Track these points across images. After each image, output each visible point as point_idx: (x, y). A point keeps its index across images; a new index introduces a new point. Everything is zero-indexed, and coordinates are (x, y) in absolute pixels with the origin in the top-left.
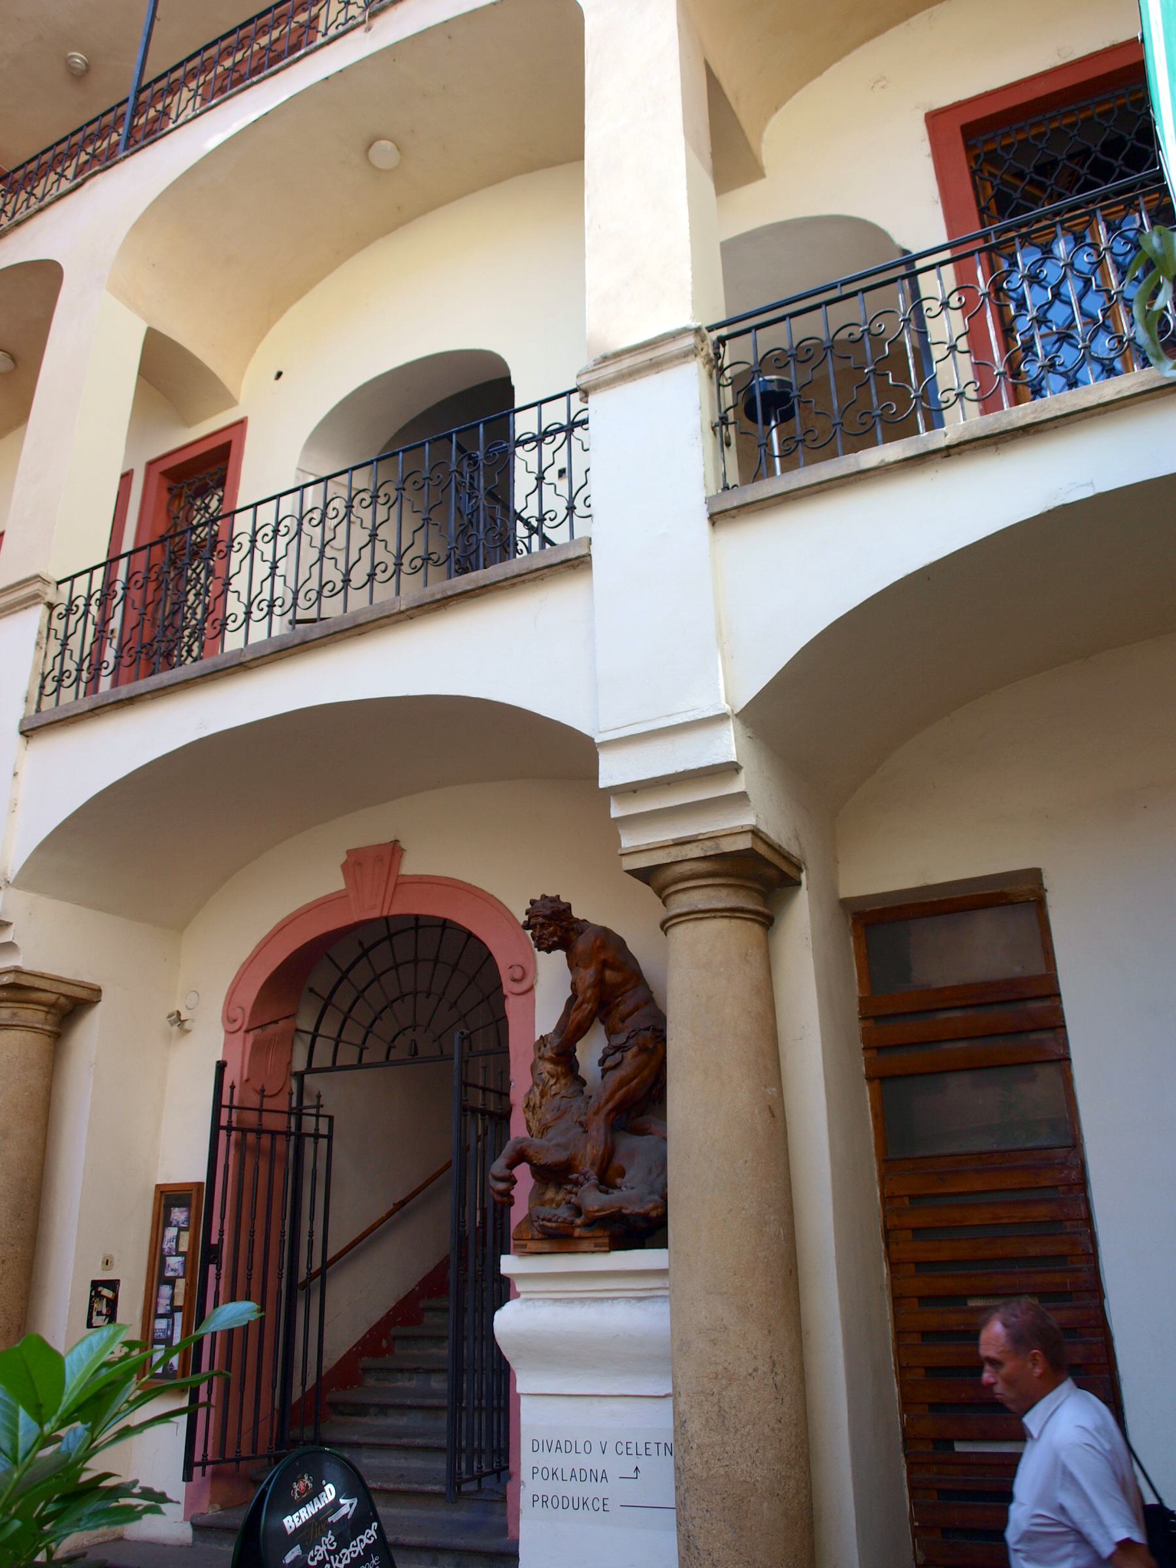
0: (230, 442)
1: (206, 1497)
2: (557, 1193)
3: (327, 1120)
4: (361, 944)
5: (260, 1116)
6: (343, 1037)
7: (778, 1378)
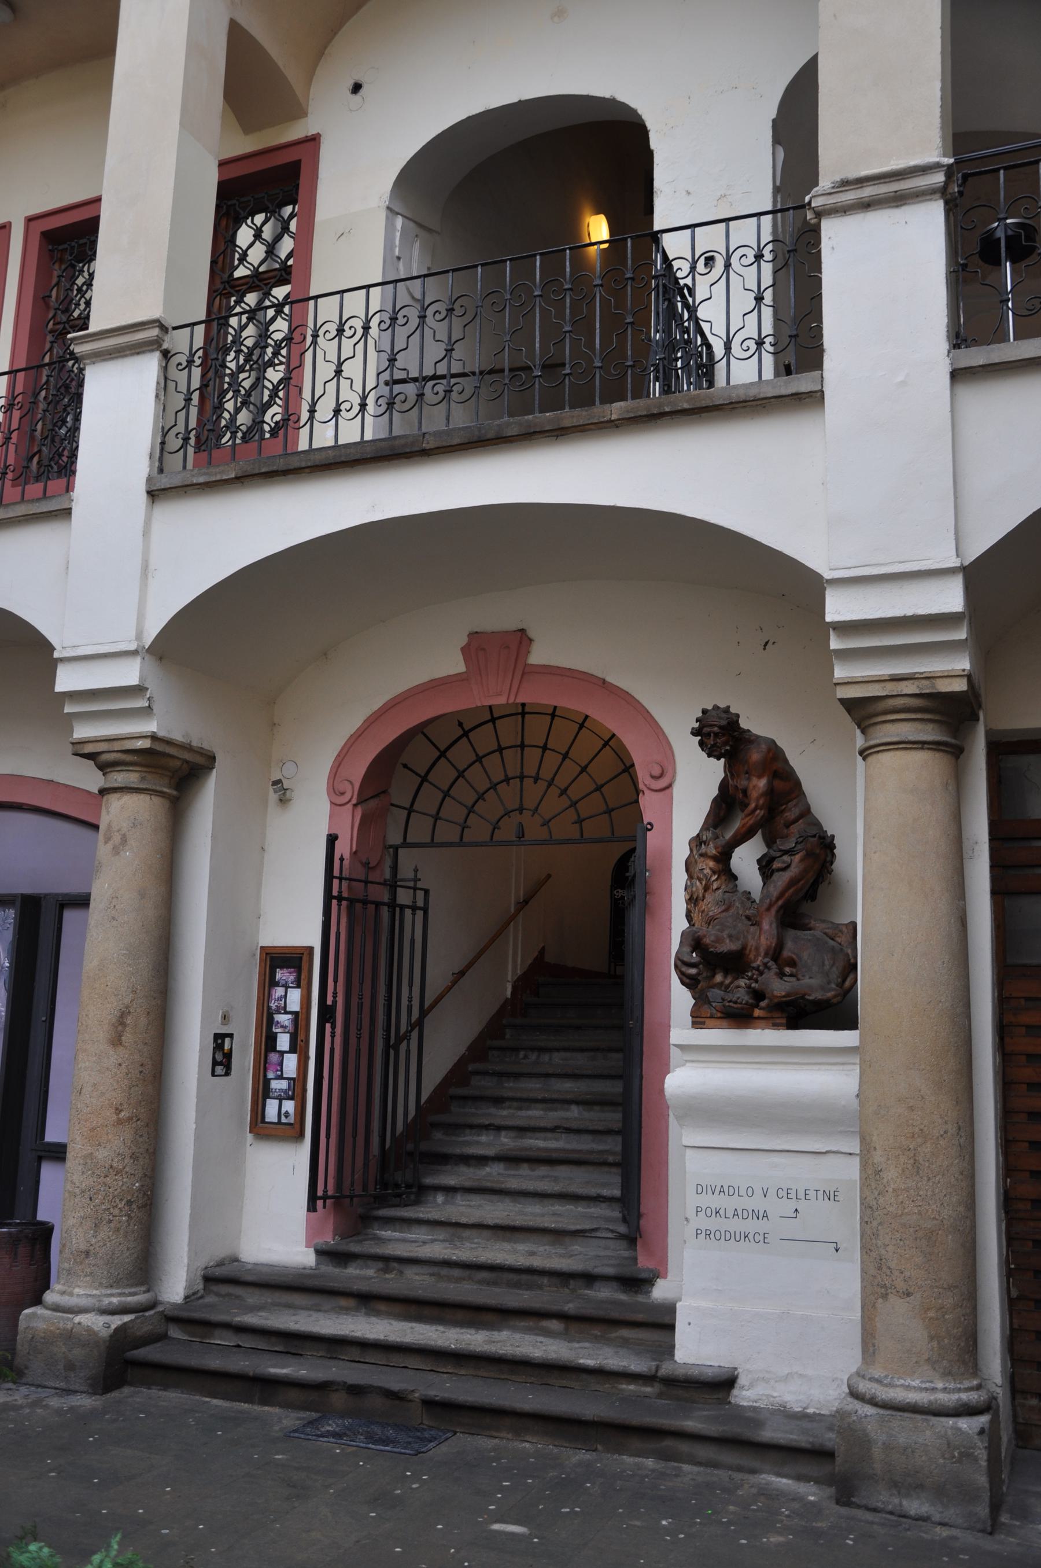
0: (300, 161)
1: (330, 1227)
2: (725, 977)
3: (423, 892)
4: (460, 724)
5: (366, 886)
6: (414, 808)
7: (962, 1140)
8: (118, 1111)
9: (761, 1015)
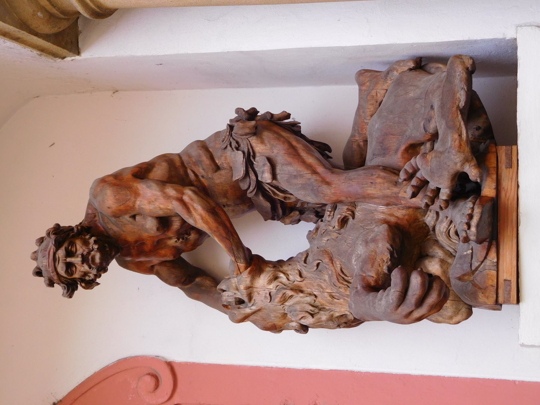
9: (494, 185)
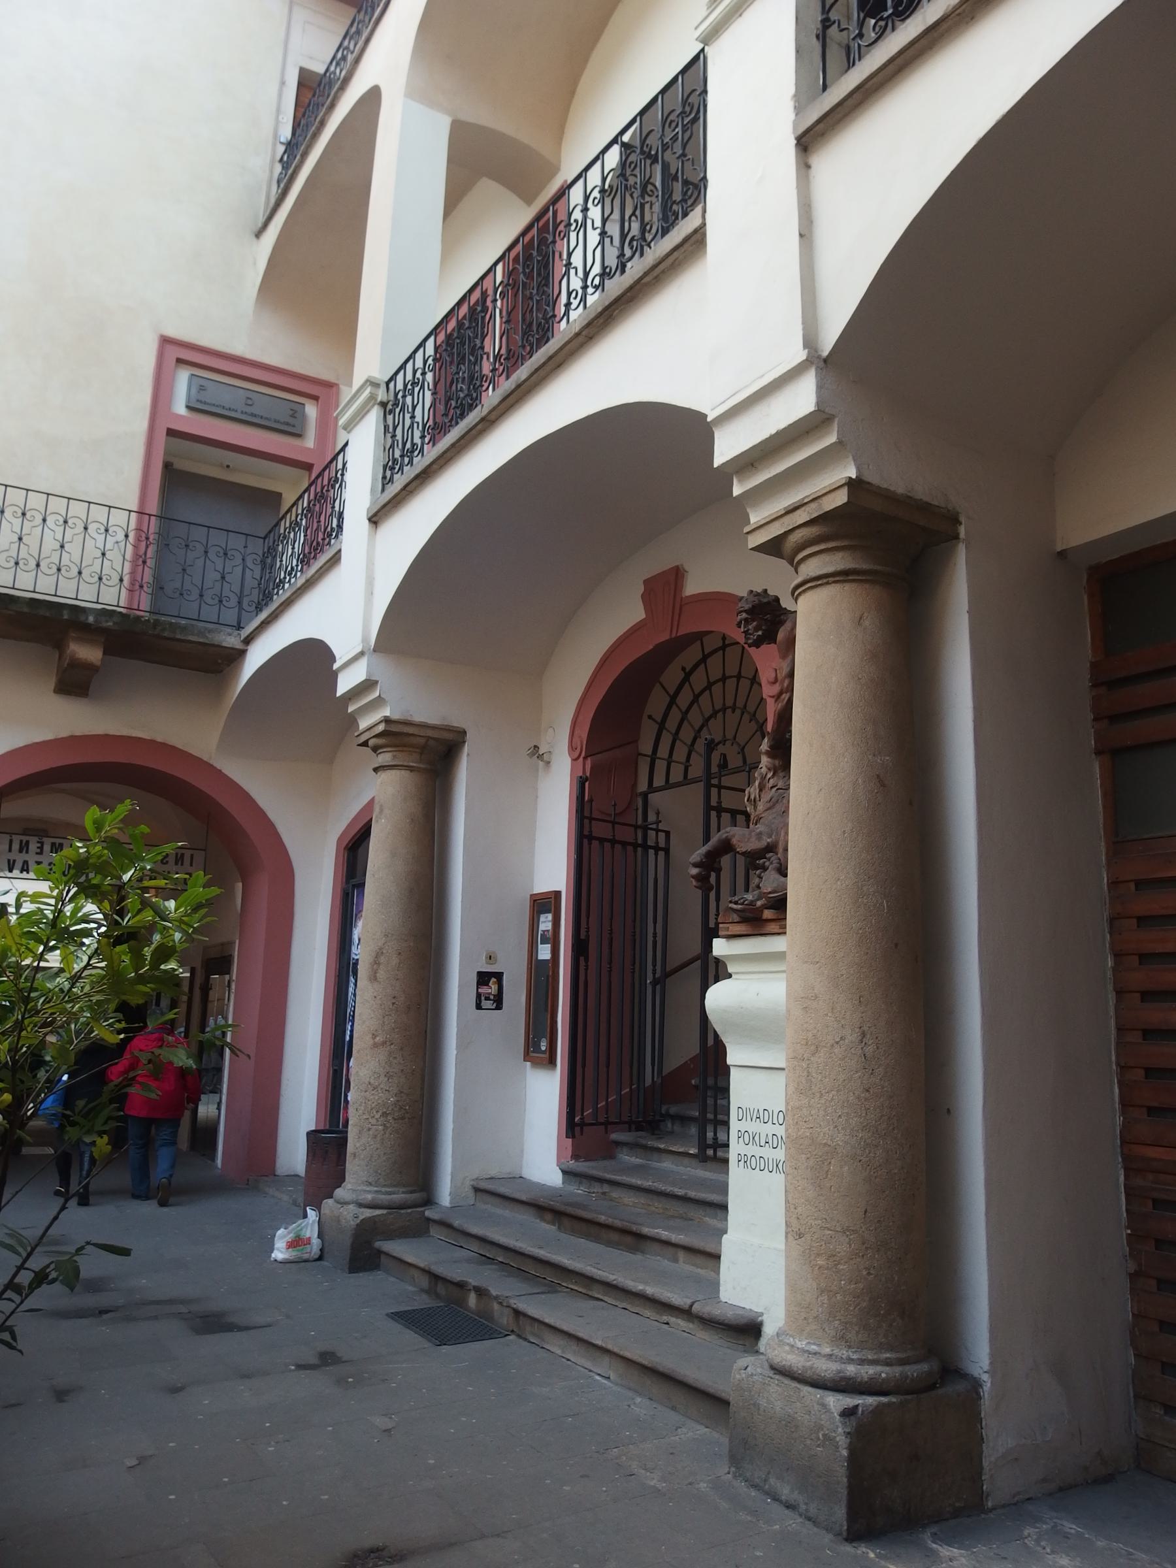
4: (683, 669)
6: (674, 758)
8: (374, 1036)
